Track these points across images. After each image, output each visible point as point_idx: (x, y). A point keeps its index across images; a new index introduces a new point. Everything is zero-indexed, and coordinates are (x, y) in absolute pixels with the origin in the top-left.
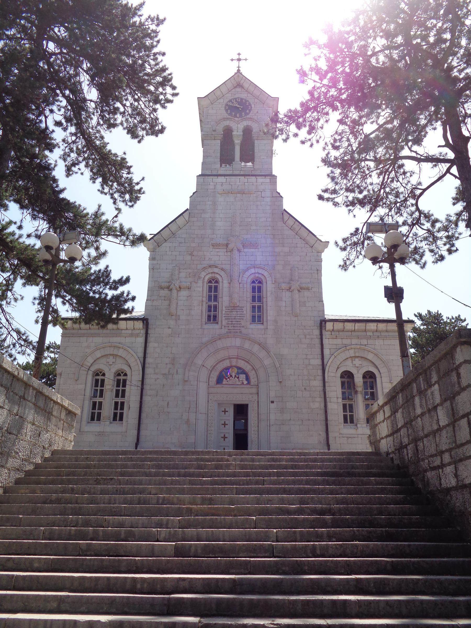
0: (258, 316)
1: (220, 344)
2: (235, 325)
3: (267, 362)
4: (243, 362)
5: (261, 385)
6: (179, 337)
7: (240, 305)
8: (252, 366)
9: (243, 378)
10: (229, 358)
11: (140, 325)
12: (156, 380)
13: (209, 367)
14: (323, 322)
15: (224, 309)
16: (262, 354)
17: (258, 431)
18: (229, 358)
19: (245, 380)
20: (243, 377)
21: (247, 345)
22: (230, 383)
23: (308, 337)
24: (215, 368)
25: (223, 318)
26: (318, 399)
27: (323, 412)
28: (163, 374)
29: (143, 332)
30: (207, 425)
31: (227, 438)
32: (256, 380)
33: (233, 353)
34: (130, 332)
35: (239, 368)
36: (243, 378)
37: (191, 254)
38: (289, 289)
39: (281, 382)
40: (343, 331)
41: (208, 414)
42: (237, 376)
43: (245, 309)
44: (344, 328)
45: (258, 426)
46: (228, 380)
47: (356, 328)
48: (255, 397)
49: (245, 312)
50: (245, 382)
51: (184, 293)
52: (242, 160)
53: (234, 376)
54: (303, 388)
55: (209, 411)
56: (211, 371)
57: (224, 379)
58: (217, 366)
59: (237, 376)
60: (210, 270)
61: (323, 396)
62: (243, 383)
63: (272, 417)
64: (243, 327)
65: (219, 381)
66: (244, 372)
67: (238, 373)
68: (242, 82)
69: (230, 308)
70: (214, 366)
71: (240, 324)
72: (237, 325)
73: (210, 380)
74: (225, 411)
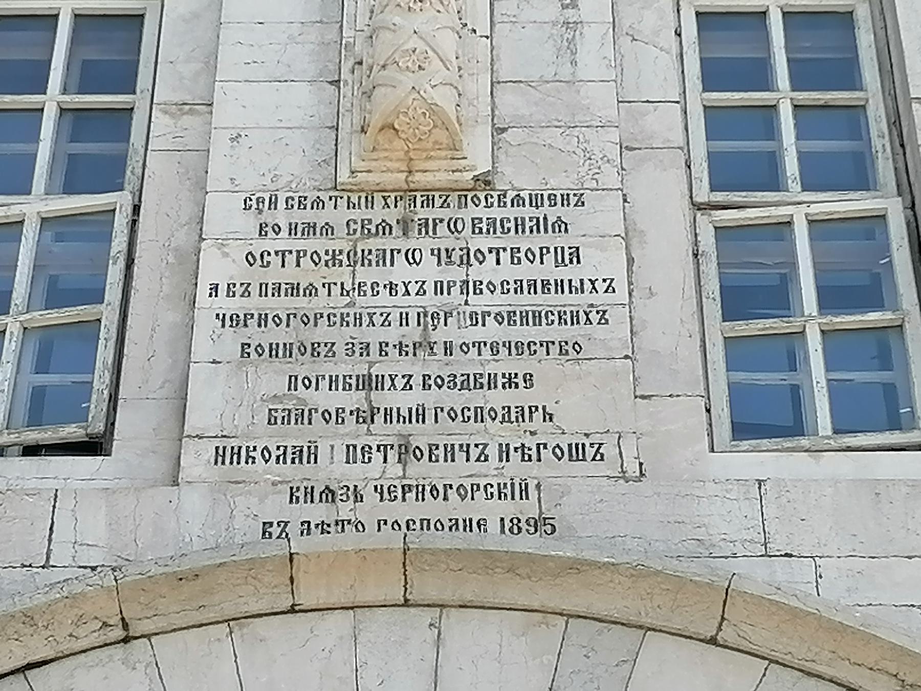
2: (422, 435)
7: (517, 176)
15: (226, 215)
43: (595, 221)
64: (576, 453)
69: (336, 215)
72: (472, 434)
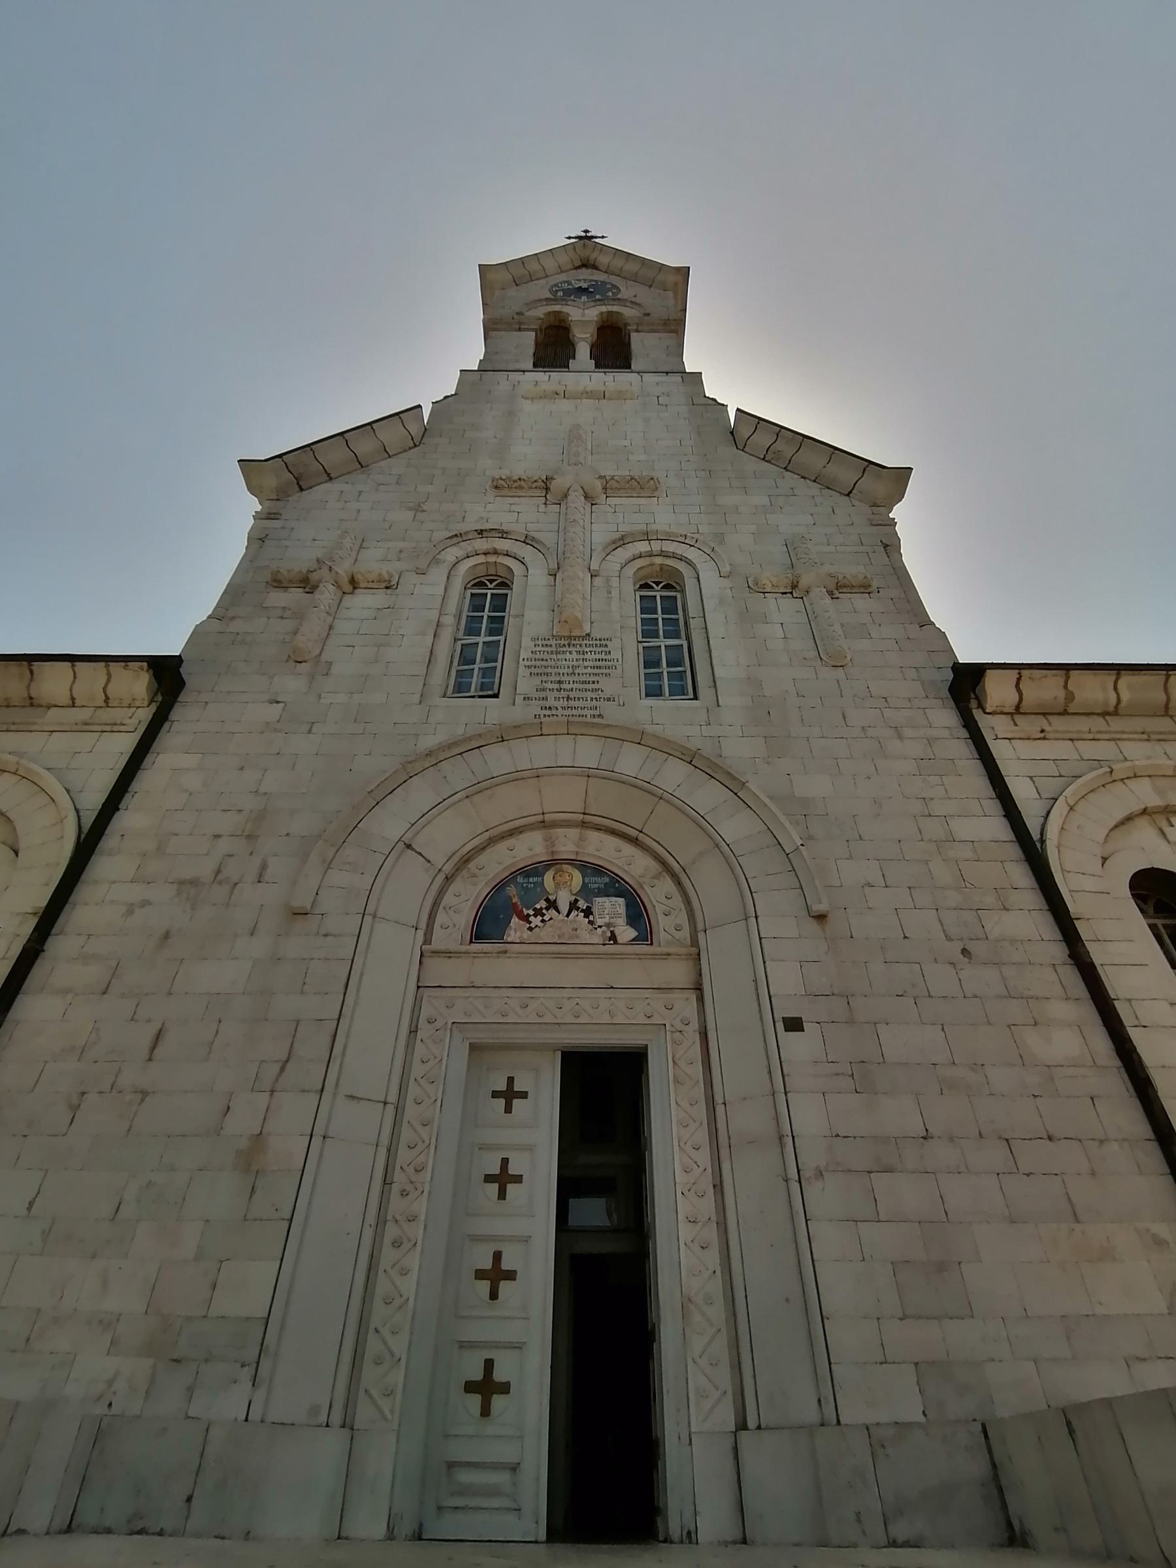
0: (672, 667)
2: (572, 695)
3: (735, 828)
4: (612, 841)
5: (711, 942)
6: (310, 732)
7: (596, 634)
9: (614, 915)
11: (140, 684)
12: (130, 911)
13: (439, 860)
14: (967, 682)
15: (527, 642)
16: (707, 797)
17: (722, 1225)
18: (543, 825)
20: (611, 908)
21: (630, 761)
22: (545, 934)
23: (908, 732)
24: (471, 865)
26: (1060, 1010)
27: (1117, 1084)
28: (181, 883)
29: (145, 715)
30: (387, 1182)
31: (518, 1179)
32: (683, 919)
33: (564, 798)
34: (84, 714)
35: (588, 868)
36: (614, 915)
37: (418, 508)
38: (793, 589)
39: (821, 918)
40: (1065, 713)
41: (399, 1110)
42: (582, 904)
44: (1070, 697)
45: (719, 1187)
46: (535, 921)
47: (1125, 696)
48: (686, 1005)
49: (617, 654)
50: (626, 933)
51: (364, 602)
53: (564, 906)
54: (957, 947)
55: (413, 1091)
56: (449, 879)
57: (515, 920)
58: (482, 859)
59: (582, 904)
60: (482, 544)
61: (1081, 990)
63: (808, 1118)
64: (609, 700)
65: (488, 925)
66: (617, 887)
67: (586, 891)
68: (593, 256)
70: (466, 860)
73: (441, 918)
74: (510, 1095)
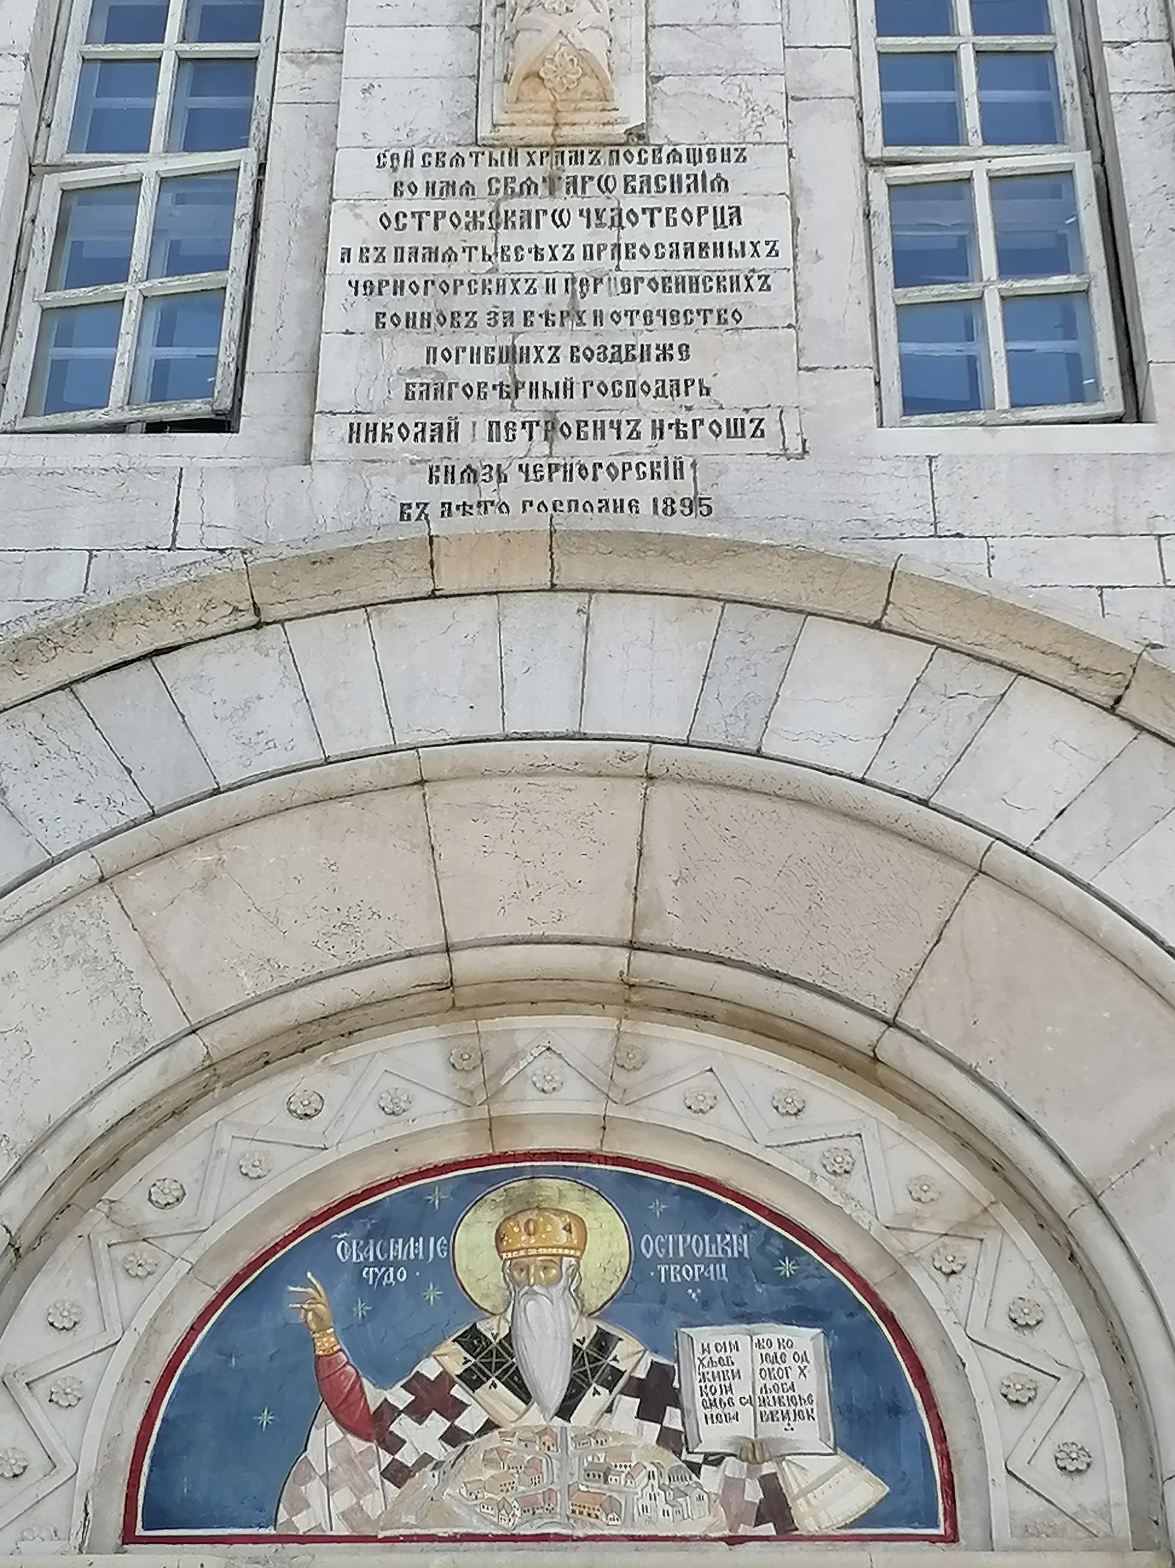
1: (247, 706)
2: (569, 411)
7: (672, 129)
8: (967, 1140)
9: (777, 1405)
10: (449, 998)
15: (358, 174)
18: (449, 999)
19: (811, 1434)
20: (762, 1378)
21: (837, 706)
24: (127, 1189)
25: (341, 310)
33: (536, 877)
36: (777, 1405)
42: (631, 1356)
43: (757, 180)
46: (422, 1437)
49: (765, 222)
50: (835, 1488)
52: (893, 188)
58: (175, 1160)
59: (631, 1356)
62: (775, 1509)
64: (735, 429)
66: (782, 1271)
67: (647, 1298)
71: (677, 388)
